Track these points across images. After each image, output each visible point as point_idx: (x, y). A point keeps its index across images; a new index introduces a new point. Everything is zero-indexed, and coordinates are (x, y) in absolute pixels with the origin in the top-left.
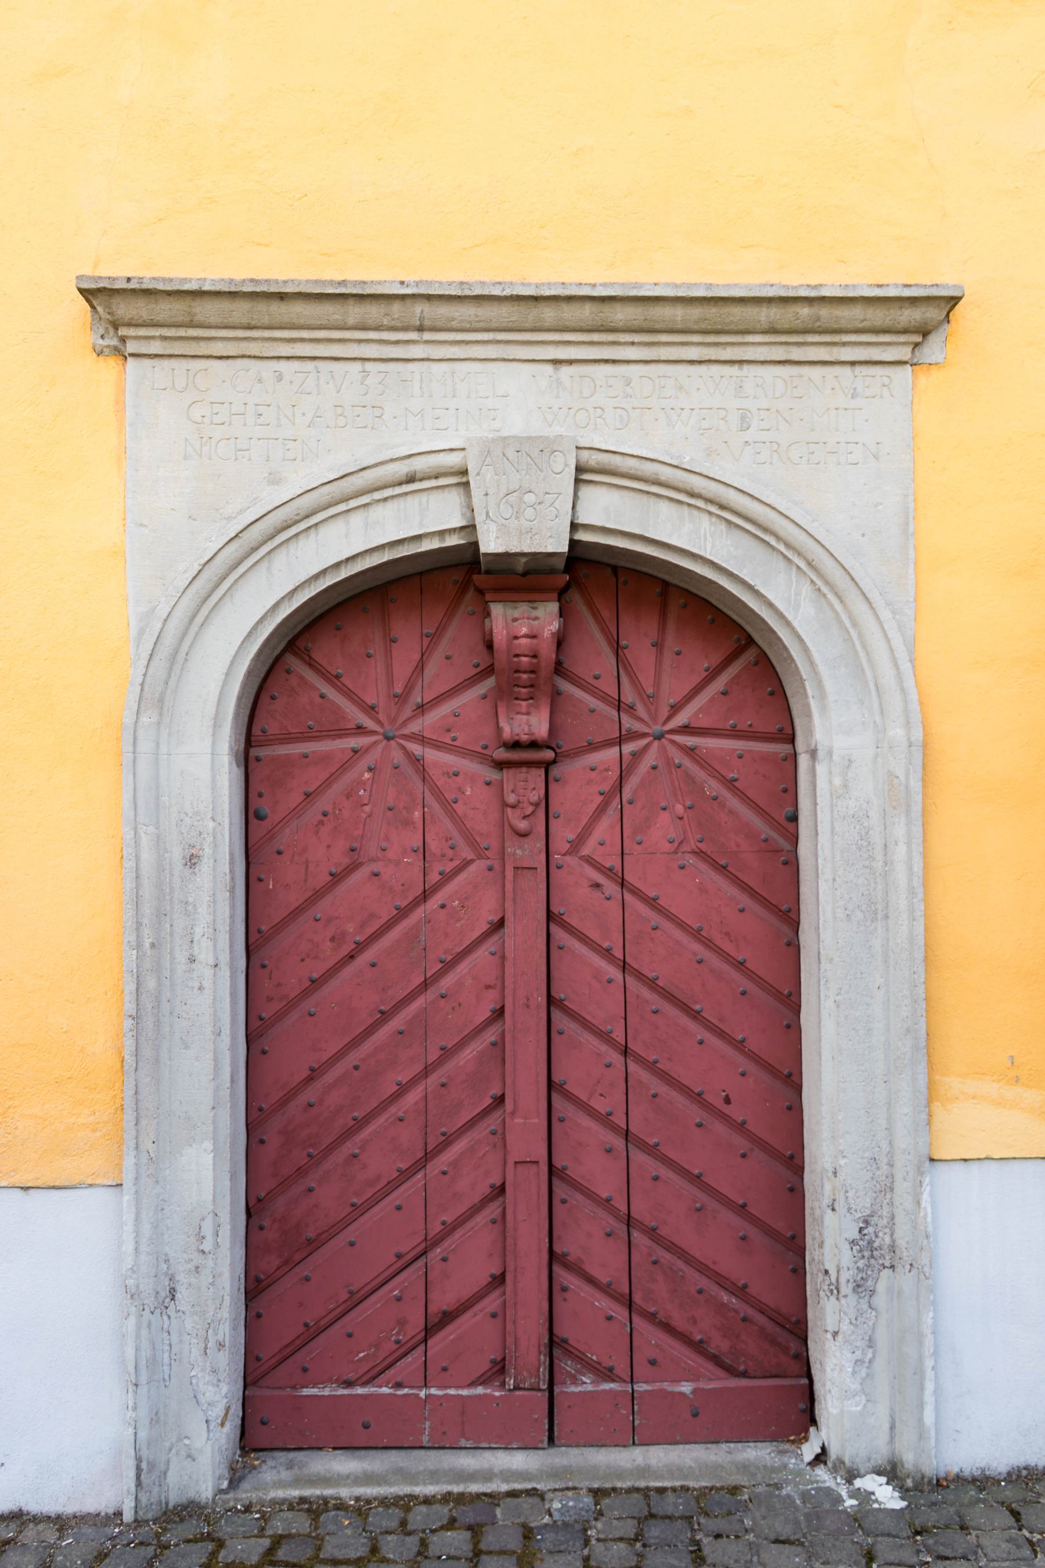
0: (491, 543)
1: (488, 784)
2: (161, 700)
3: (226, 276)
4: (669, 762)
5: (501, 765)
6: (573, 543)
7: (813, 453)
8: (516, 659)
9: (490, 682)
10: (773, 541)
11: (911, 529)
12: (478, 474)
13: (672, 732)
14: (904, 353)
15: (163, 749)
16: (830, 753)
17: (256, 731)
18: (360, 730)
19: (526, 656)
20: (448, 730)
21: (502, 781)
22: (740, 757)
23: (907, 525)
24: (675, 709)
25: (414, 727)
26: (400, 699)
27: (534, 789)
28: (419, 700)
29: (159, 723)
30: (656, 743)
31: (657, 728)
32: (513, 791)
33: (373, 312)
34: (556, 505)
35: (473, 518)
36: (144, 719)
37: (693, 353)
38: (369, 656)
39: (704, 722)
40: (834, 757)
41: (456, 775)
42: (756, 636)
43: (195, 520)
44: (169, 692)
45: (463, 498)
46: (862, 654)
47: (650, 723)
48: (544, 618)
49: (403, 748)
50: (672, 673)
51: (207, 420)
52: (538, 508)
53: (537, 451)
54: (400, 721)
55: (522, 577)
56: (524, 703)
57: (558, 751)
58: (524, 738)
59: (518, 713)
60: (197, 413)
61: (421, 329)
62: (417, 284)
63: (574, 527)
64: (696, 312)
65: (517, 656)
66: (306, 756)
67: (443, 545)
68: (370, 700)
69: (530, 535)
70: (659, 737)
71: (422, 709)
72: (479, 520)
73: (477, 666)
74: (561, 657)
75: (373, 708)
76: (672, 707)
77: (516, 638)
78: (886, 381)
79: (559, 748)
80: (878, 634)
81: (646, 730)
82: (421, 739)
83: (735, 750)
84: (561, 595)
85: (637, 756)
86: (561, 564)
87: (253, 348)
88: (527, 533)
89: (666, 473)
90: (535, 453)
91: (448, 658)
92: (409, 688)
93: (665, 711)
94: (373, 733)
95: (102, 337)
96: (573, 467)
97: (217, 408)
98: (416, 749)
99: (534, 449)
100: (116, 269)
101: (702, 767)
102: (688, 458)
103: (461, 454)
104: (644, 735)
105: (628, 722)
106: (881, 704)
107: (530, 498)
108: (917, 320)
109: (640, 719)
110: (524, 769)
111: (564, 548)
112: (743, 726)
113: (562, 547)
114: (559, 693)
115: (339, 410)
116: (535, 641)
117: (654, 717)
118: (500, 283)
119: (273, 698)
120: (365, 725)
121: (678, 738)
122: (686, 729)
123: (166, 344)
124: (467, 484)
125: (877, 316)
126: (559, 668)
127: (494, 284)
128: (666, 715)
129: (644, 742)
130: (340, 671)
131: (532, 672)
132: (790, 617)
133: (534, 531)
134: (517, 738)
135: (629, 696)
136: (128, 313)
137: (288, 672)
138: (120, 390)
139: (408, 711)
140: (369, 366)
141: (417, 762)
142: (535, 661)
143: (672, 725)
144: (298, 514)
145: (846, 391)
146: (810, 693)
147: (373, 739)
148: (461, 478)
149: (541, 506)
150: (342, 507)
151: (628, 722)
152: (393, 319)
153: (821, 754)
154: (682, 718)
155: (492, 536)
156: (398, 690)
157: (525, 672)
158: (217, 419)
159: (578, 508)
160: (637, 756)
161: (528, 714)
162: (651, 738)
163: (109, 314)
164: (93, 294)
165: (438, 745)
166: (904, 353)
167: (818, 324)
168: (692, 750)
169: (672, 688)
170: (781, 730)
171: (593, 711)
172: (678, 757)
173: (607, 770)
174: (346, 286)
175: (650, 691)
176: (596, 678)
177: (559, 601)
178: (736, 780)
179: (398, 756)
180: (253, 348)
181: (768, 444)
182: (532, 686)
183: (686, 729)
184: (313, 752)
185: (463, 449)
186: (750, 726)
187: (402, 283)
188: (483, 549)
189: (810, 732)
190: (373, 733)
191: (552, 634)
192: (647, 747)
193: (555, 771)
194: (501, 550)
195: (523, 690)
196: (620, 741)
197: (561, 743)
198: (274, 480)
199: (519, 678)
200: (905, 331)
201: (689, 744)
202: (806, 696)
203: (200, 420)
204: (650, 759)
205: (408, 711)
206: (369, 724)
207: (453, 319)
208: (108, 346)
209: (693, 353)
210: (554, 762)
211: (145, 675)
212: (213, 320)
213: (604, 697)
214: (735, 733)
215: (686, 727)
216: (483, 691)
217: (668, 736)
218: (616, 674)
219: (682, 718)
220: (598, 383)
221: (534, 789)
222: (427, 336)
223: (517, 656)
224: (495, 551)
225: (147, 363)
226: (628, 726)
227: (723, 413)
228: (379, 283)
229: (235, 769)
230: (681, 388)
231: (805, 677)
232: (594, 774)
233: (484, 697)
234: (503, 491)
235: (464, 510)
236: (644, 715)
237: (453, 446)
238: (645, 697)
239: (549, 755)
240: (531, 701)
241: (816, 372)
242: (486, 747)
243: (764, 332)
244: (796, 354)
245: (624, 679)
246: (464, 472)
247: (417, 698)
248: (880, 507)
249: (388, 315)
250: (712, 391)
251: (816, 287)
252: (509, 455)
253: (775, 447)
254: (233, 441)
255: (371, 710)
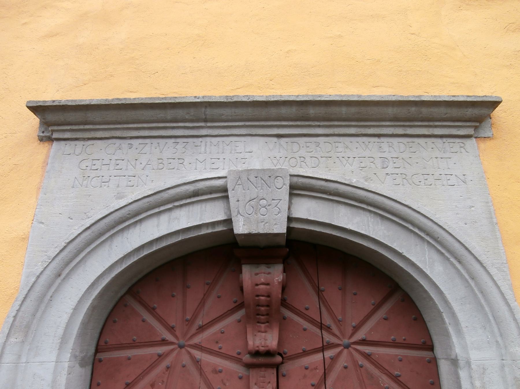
0: (241, 228)
1: (241, 378)
2: (28, 327)
3: (105, 98)
4: (355, 362)
5: (249, 366)
6: (289, 229)
7: (426, 180)
8: (257, 298)
9: (241, 313)
10: (411, 227)
11: (495, 220)
12: (233, 190)
13: (355, 343)
14: (471, 131)
15: (24, 359)
16: (468, 363)
17: (102, 343)
18: (164, 342)
19: (263, 296)
20: (217, 342)
21: (249, 376)
22: (401, 360)
23: (492, 218)
24: (356, 329)
25: (196, 340)
26: (190, 322)
27: (269, 382)
28: (201, 323)
29: (23, 342)
30: (346, 351)
31: (346, 341)
32: (256, 384)
33: (180, 113)
34: (278, 206)
35: (231, 215)
36: (12, 340)
37: (353, 131)
38: (173, 296)
39: (375, 337)
40: (473, 366)
41: (220, 372)
42: (401, 284)
43: (71, 219)
44: (35, 321)
45: (225, 204)
46: (480, 296)
47: (341, 337)
48: (276, 274)
49: (189, 353)
50: (352, 307)
51: (88, 168)
52: (268, 208)
53: (267, 176)
54: (189, 336)
55: (259, 250)
56: (263, 325)
57: (284, 356)
58: (262, 349)
59: (259, 331)
60: (83, 166)
61: (206, 121)
62: (203, 97)
63: (290, 219)
64: (353, 110)
65: (258, 296)
66: (129, 359)
67: (214, 231)
68: (172, 324)
69: (263, 223)
70: (347, 347)
71: (202, 329)
72: (234, 214)
73: (235, 302)
74: (286, 297)
75: (173, 328)
76: (354, 327)
77: (257, 285)
78: (462, 145)
79: (285, 354)
80: (490, 284)
81: (339, 342)
82: (198, 347)
83: (397, 355)
84: (285, 261)
85: (334, 359)
86: (283, 242)
87: (118, 134)
88: (262, 222)
89: (342, 188)
90: (266, 178)
91: (219, 297)
92: (195, 316)
93: (350, 331)
94: (172, 343)
95: (43, 132)
96: (288, 185)
97: (95, 162)
98: (197, 354)
99: (267, 176)
100: (50, 95)
101: (376, 366)
102: (355, 180)
103: (224, 180)
104: (338, 345)
105: (328, 338)
106: (499, 329)
107: (263, 202)
108: (470, 117)
109: (334, 335)
110: (263, 369)
111: (284, 231)
112: (399, 340)
113: (283, 230)
114: (284, 318)
115: (160, 161)
116: (268, 287)
117: (343, 335)
118: (247, 96)
119: (115, 322)
120: (167, 339)
121: (359, 347)
122: (363, 342)
123: (73, 133)
124: (227, 197)
125: (455, 112)
126: (284, 303)
127: (244, 96)
128: (350, 332)
129: (338, 350)
130: (155, 305)
131: (268, 306)
132: (428, 272)
133: (265, 222)
134: (257, 349)
135: (327, 320)
136: (62, 121)
137: (126, 306)
138: (47, 157)
139: (193, 330)
140: (178, 140)
141: (197, 362)
142: (268, 299)
143: (355, 339)
144: (129, 214)
145: (440, 149)
146: (447, 321)
147: (172, 347)
148: (222, 193)
149: (269, 207)
150: (157, 210)
151: (328, 338)
152: (191, 116)
153: (462, 363)
154: (360, 335)
155: (241, 223)
156: (188, 317)
157: (263, 306)
158: (94, 167)
159: (292, 209)
160: (334, 359)
161: (265, 332)
162: (342, 348)
163: (44, 119)
164: (37, 109)
165: (210, 352)
166: (471, 131)
167: (420, 116)
168: (369, 355)
169: (353, 317)
170: (424, 343)
171: (305, 330)
172: (361, 361)
173: (316, 369)
174: (166, 99)
175: (340, 318)
176: (307, 309)
177: (283, 263)
178: (399, 376)
179: (186, 360)
180: (118, 134)
181: (399, 175)
182: (267, 315)
183: (363, 342)
184: (135, 356)
185: (226, 177)
186: (404, 340)
187: (195, 97)
188: (236, 231)
189: (449, 346)
190: (172, 343)
191: (279, 283)
192: (340, 353)
193: (284, 369)
194: (246, 232)
195: (262, 317)
196: (323, 349)
197: (286, 350)
198: (119, 197)
199: (259, 309)
200: (469, 120)
201: (367, 351)
202: (444, 322)
203: (85, 168)
204: (342, 361)
205: (193, 330)
206: (170, 337)
207: (223, 115)
208: (46, 136)
209: (353, 131)
210: (282, 363)
211: (18, 311)
212: (98, 119)
213: (312, 321)
214: (395, 345)
215: (364, 340)
216: (239, 318)
217: (352, 346)
218: (318, 306)
219: (360, 335)
220: (301, 146)
221: (269, 382)
222: (209, 124)
223: (258, 296)
224: (243, 233)
225: (63, 143)
226: (328, 339)
227: (372, 160)
228: (184, 97)
229: (78, 369)
230: (347, 147)
231: (442, 311)
232: (307, 372)
233: (239, 321)
234: (248, 199)
235: (226, 210)
236: (337, 332)
237: (220, 175)
238: (337, 321)
239: (279, 359)
240: (267, 324)
241: (422, 141)
242: (239, 354)
243: (390, 120)
244: (410, 131)
245: (323, 309)
246: (225, 190)
247: (200, 322)
248: (473, 209)
249: (188, 113)
250: (364, 149)
251: (418, 96)
252: (256, 186)
253: (404, 176)
254: (101, 177)
255: (171, 329)
